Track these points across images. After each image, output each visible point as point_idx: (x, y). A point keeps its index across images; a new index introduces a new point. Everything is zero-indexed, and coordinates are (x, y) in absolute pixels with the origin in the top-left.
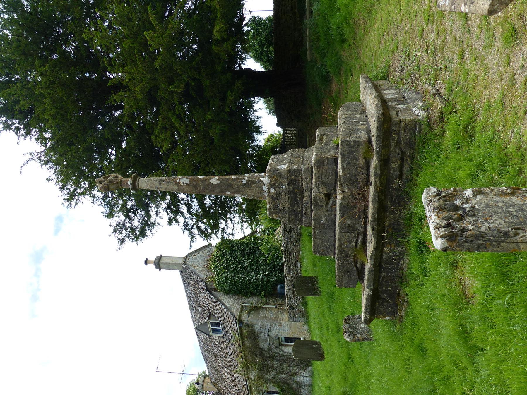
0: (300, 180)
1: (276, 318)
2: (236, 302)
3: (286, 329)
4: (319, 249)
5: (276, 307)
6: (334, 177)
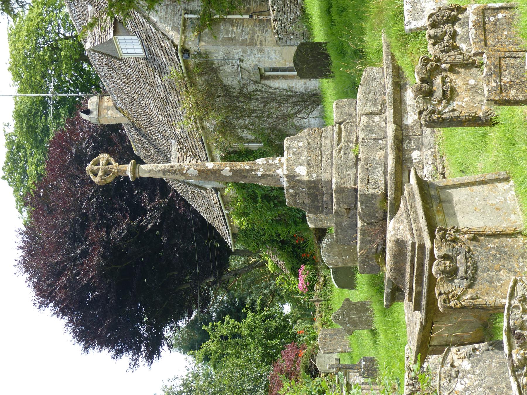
0: (320, 187)
1: (252, 39)
2: (170, 11)
3: (273, 56)
4: (342, 241)
5: (251, 16)
6: (355, 199)
